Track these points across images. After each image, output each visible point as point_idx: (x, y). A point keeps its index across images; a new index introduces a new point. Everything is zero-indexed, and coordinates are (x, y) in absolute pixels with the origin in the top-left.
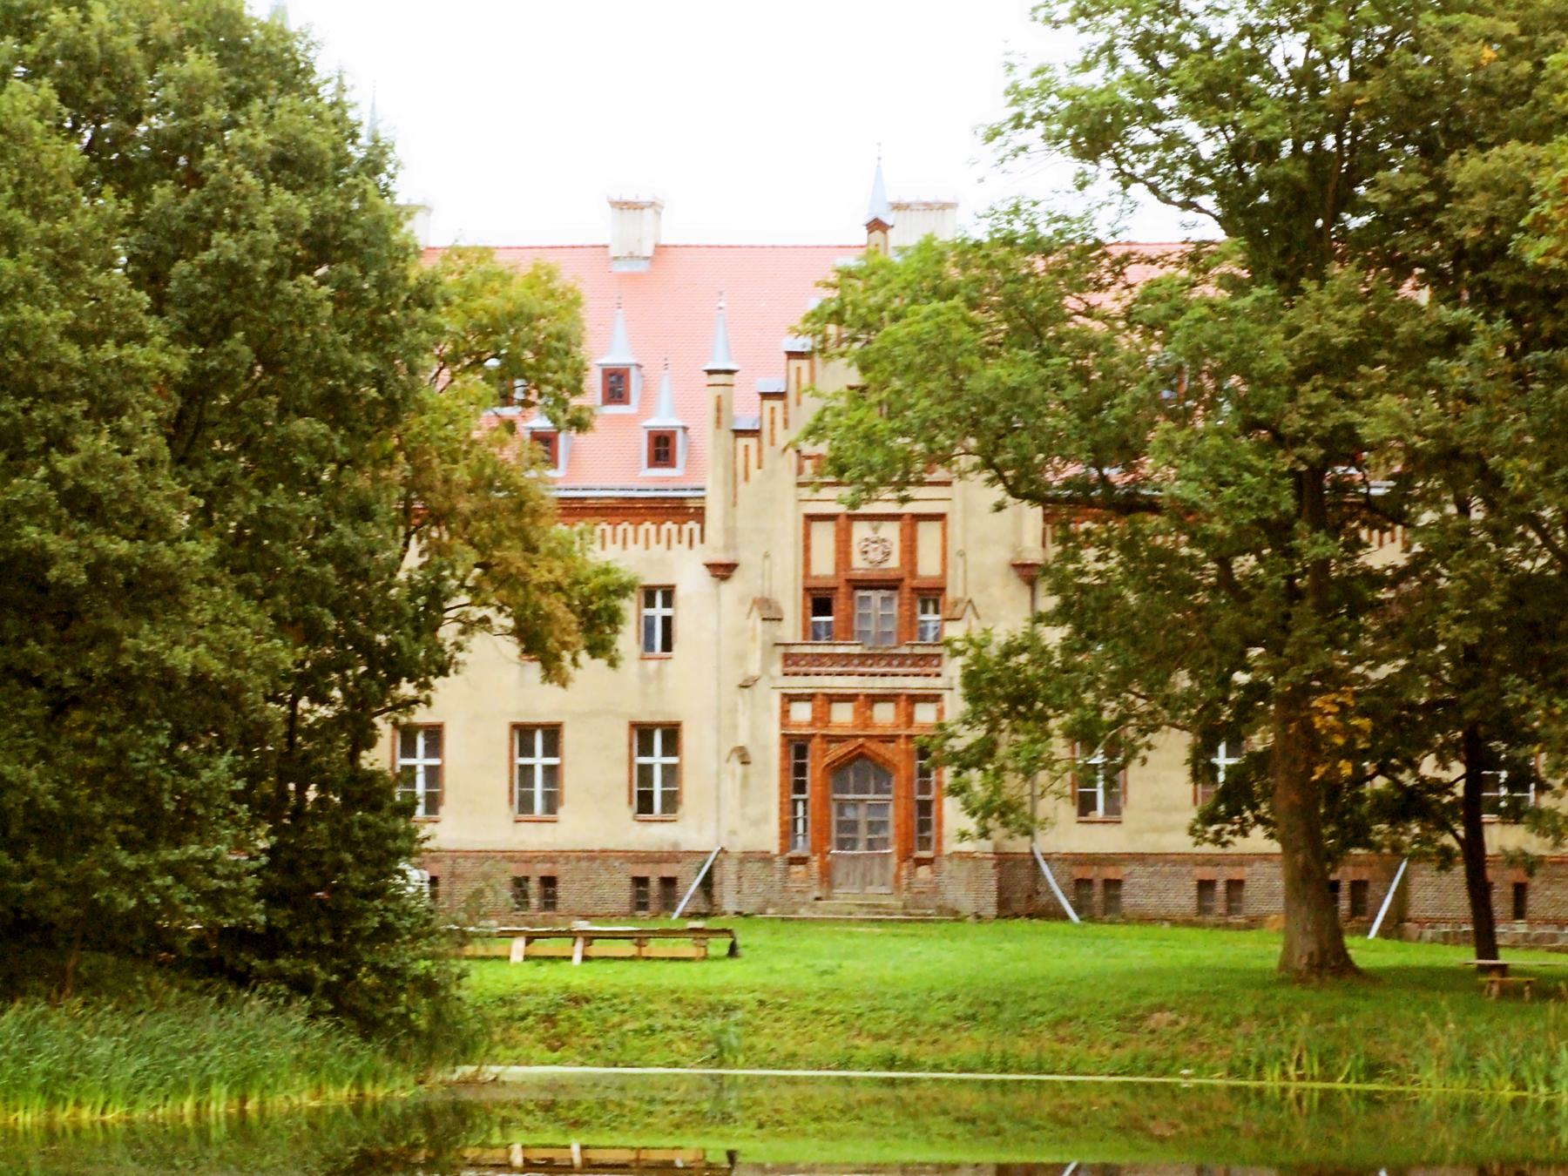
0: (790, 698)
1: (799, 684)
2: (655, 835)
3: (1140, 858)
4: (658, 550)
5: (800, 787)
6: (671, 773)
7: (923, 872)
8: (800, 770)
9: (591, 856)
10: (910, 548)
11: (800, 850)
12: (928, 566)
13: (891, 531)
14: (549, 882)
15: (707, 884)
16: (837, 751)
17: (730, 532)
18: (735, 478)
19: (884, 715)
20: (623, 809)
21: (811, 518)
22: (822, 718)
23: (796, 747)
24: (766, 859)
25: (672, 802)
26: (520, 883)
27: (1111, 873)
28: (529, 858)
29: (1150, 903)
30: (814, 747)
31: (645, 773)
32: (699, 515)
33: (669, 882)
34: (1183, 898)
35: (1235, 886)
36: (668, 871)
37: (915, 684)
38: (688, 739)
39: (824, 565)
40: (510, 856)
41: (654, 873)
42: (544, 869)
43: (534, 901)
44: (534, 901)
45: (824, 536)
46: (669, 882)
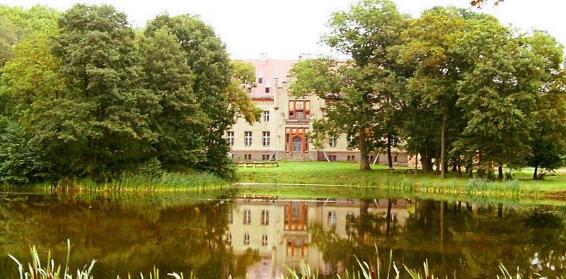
1: (288, 126)
2: (266, 148)
3: (339, 152)
9: (256, 152)
10: (305, 105)
12: (307, 108)
19: (301, 130)
23: (287, 135)
24: (282, 152)
25: (268, 143)
35: (353, 156)
37: (305, 126)
38: (271, 134)
39: (292, 108)
41: (266, 154)
43: (442, 204)
44: (442, 204)
45: (292, 103)
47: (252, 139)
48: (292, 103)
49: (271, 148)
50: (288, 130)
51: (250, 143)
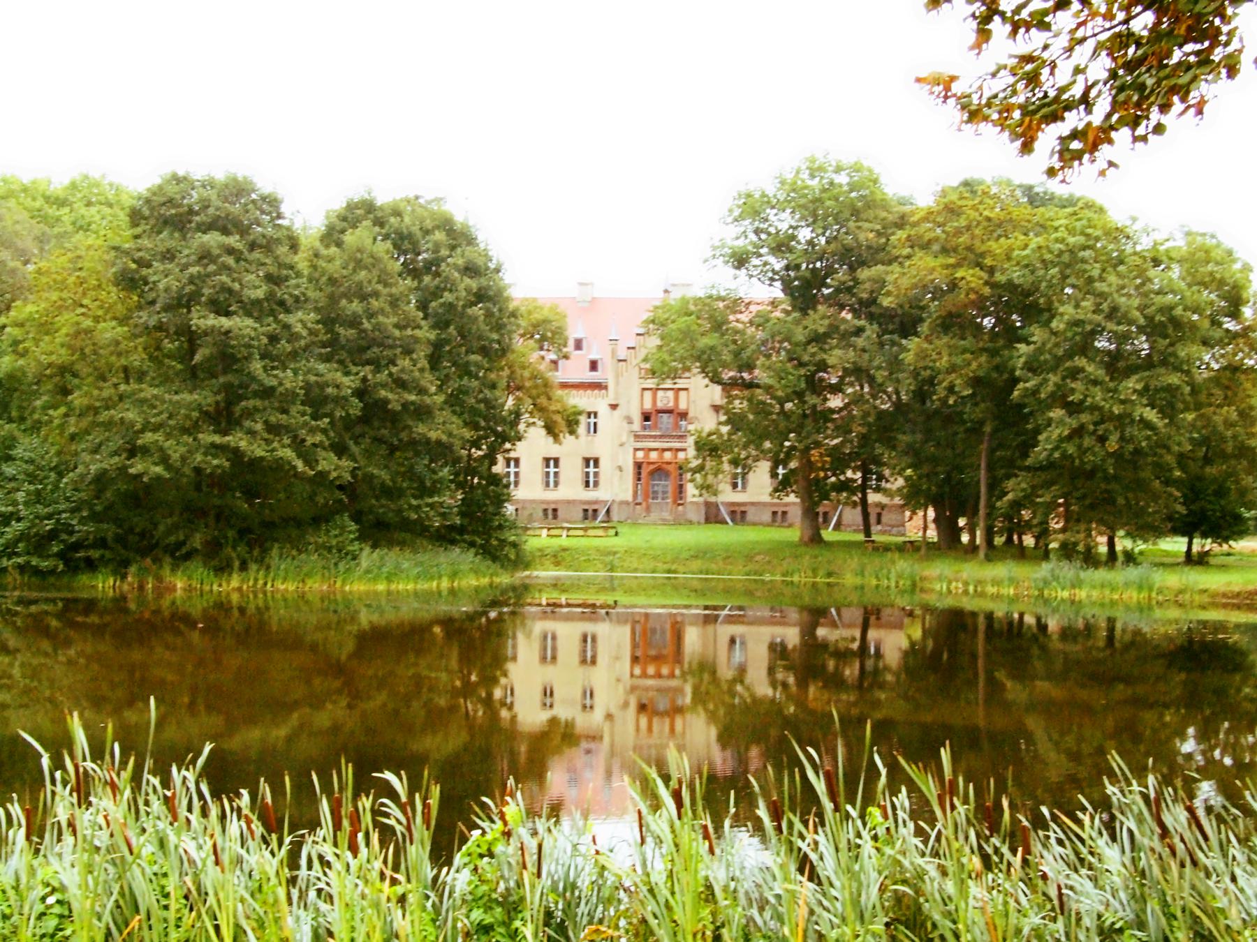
0: (637, 450)
1: (639, 445)
2: (591, 495)
3: (753, 504)
4: (592, 399)
5: (639, 479)
6: (596, 474)
7: (680, 508)
8: (639, 473)
9: (569, 502)
10: (677, 399)
11: (639, 500)
13: (670, 394)
14: (555, 510)
15: (608, 511)
16: (652, 467)
17: (617, 393)
18: (617, 376)
19: (668, 455)
20: (581, 486)
21: (644, 389)
22: (646, 456)
23: (638, 466)
24: (627, 503)
25: (596, 484)
26: (545, 510)
27: (743, 509)
28: (548, 502)
29: (756, 519)
30: (644, 466)
31: (587, 474)
32: (606, 388)
33: (595, 511)
34: (767, 517)
35: (784, 513)
36: (595, 507)
38: (602, 463)
39: (648, 406)
40: (543, 502)
41: (591, 508)
42: (553, 506)
45: (648, 395)
46: (595, 511)
47: (521, 475)
48: (648, 395)
49: (604, 494)
50: (640, 454)
51: (556, 484)
